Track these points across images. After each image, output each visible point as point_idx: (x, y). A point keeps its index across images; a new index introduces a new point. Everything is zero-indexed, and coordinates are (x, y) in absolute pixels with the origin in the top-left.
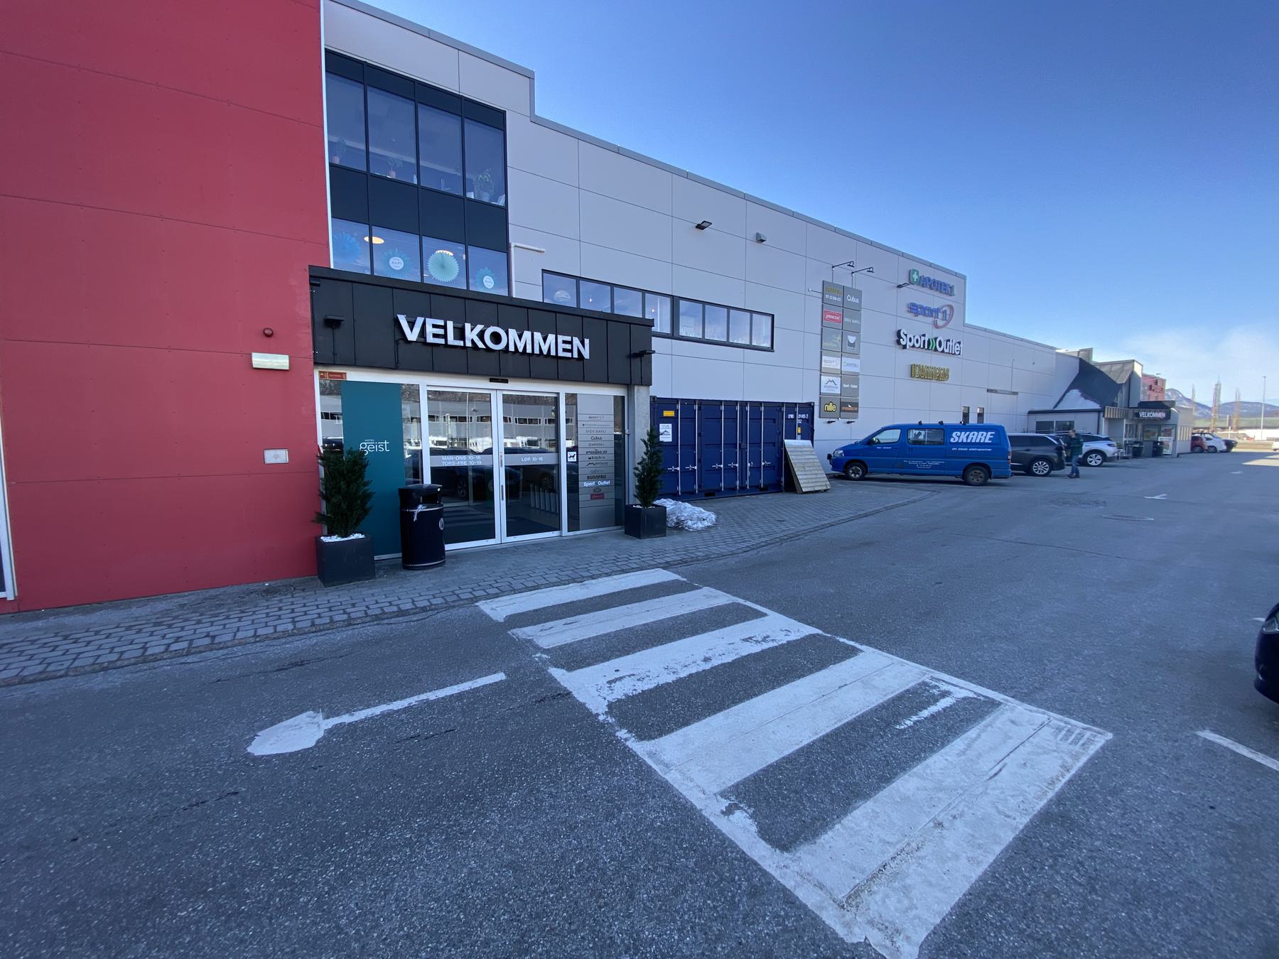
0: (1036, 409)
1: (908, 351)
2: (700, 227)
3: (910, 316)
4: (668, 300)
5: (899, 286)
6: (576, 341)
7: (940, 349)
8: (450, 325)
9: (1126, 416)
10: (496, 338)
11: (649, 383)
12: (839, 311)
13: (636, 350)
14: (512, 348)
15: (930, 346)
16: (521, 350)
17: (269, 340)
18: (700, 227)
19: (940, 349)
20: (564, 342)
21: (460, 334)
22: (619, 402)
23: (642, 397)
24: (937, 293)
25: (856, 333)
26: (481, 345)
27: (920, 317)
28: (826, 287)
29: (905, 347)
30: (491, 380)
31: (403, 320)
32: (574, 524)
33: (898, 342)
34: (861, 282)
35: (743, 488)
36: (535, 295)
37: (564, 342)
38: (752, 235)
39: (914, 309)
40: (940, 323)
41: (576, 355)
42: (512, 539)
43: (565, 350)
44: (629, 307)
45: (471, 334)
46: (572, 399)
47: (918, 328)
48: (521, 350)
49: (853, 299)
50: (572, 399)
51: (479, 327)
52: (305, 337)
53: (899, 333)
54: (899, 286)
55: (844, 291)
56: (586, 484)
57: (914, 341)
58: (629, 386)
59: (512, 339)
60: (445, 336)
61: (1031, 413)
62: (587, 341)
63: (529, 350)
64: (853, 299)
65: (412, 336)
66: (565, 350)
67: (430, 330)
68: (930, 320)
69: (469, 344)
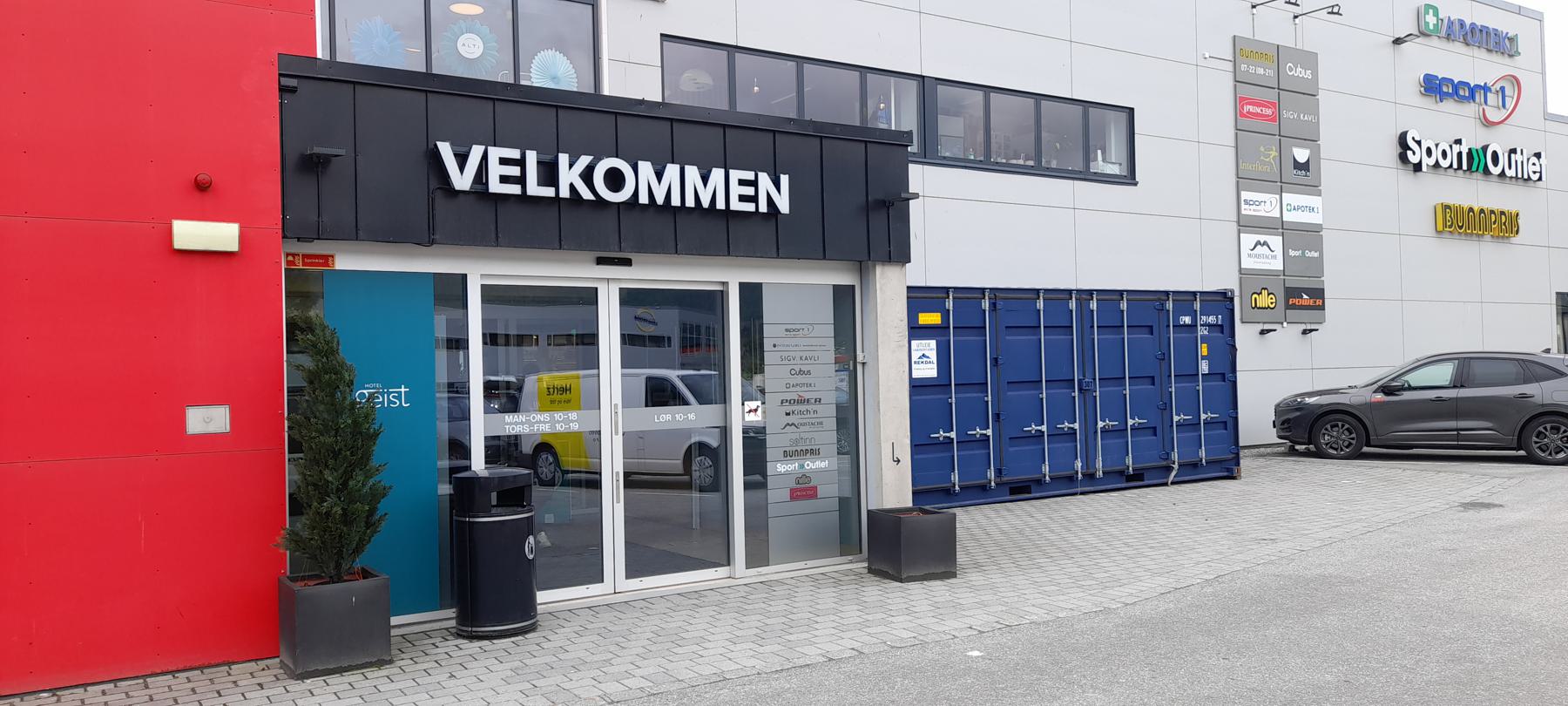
1: (1426, 176)
3: (1428, 102)
5: (1398, 41)
7: (1496, 171)
8: (532, 158)
10: (615, 179)
11: (899, 254)
14: (644, 199)
15: (1475, 163)
17: (203, 198)
19: (1496, 171)
21: (549, 174)
22: (843, 298)
23: (888, 290)
24: (1483, 54)
25: (1311, 140)
26: (586, 194)
27: (1449, 106)
29: (1418, 167)
30: (600, 261)
31: (445, 150)
32: (757, 557)
33: (1403, 158)
39: (1433, 87)
40: (1494, 115)
41: (763, 208)
42: (636, 583)
45: (569, 176)
46: (752, 295)
49: (1299, 72)
50: (752, 295)
51: (584, 161)
52: (268, 188)
54: (1398, 41)
56: (782, 468)
57: (1437, 154)
59: (646, 181)
60: (521, 180)
62: (784, 179)
63: (676, 201)
64: (1299, 72)
65: (462, 181)
67: (495, 170)
68: (1471, 109)
69: (565, 193)
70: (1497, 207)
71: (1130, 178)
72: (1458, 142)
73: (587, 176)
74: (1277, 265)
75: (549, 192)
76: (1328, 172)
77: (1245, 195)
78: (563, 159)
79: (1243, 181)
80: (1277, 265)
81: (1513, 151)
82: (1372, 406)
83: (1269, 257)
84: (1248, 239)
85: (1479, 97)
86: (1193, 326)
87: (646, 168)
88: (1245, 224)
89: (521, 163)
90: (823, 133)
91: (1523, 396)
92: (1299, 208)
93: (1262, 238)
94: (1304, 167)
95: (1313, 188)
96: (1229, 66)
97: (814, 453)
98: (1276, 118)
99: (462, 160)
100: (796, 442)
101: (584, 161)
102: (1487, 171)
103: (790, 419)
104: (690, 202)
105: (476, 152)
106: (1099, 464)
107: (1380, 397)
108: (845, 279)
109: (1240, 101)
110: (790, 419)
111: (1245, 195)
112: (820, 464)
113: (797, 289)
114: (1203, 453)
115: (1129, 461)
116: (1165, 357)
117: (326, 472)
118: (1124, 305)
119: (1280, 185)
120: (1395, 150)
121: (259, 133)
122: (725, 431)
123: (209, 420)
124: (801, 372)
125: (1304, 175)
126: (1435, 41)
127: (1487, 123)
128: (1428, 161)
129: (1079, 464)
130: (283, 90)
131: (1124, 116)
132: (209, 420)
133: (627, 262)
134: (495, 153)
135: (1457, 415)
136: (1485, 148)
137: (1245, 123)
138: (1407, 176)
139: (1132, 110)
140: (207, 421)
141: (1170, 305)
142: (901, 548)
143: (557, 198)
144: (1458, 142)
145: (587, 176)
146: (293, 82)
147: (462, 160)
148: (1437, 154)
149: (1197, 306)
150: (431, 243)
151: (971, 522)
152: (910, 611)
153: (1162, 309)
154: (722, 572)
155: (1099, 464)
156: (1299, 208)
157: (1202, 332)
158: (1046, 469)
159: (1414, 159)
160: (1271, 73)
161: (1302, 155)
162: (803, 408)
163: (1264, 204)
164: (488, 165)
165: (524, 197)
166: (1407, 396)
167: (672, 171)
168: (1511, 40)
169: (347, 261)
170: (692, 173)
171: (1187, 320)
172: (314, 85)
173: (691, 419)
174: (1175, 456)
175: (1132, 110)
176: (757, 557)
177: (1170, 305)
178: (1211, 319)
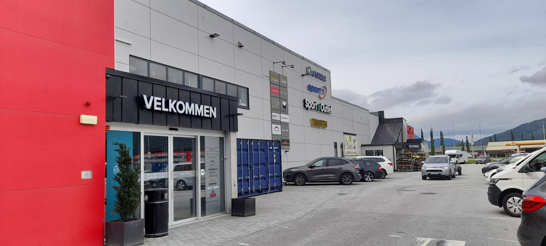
0: (364, 143)
1: (309, 111)
2: (241, 46)
3: (307, 91)
4: (196, 77)
5: (303, 75)
6: (211, 108)
7: (322, 110)
8: (164, 100)
9: (404, 148)
10: (181, 107)
11: (235, 130)
12: (278, 87)
13: (231, 113)
14: (187, 113)
15: (318, 108)
16: (190, 113)
17: (88, 107)
18: (212, 36)
19: (322, 110)
20: (158, 101)
21: (167, 106)
22: (221, 139)
23: (233, 138)
24: (319, 80)
25: (286, 100)
26: (175, 111)
27: (313, 93)
28: (272, 74)
29: (307, 109)
30: (171, 129)
31: (145, 97)
32: (204, 213)
33: (304, 106)
34: (287, 72)
35: (252, 192)
36: (126, 69)
37: (158, 101)
38: (236, 43)
39: (311, 88)
40: (322, 96)
41: (211, 116)
42: (176, 222)
43: (158, 106)
44: (232, 92)
45: (171, 106)
46: (202, 138)
47: (312, 98)
48: (190, 113)
49: (283, 82)
50: (202, 138)
51: (175, 101)
52: (103, 106)
53: (304, 100)
54: (303, 75)
55: (279, 76)
56: (209, 188)
57: (311, 105)
58: (226, 133)
59: (189, 108)
60: (161, 106)
61: (362, 146)
62: (215, 108)
63: (193, 114)
64: (283, 82)
65: (149, 106)
66: (158, 106)
67: (156, 103)
68: (317, 94)
69: (170, 111)
70: (323, 120)
71: (248, 108)
72: (315, 102)
73: (175, 106)
74: (280, 133)
75: (167, 110)
76: (290, 108)
77: (273, 114)
78: (170, 101)
79: (273, 110)
80: (280, 133)
81: (325, 106)
82: (307, 171)
83: (278, 131)
84: (274, 126)
85: (319, 91)
86: (273, 149)
87: (187, 104)
88: (273, 122)
89: (161, 101)
90: (221, 97)
91: (341, 168)
92: (284, 118)
93: (277, 126)
94: (285, 107)
95: (286, 113)
96: (269, 78)
97: (215, 184)
98: (279, 93)
99: (148, 100)
100: (212, 181)
101: (175, 101)
102: (321, 111)
103: (211, 174)
104: (196, 114)
105: (152, 98)
106: (254, 188)
107: (309, 169)
108: (221, 136)
109: (271, 88)
110: (211, 174)
111: (273, 114)
112: (217, 187)
113: (212, 137)
114: (242, 190)
115: (260, 187)
116: (267, 158)
117: (130, 189)
118: (259, 144)
119: (280, 112)
120: (303, 104)
121: (100, 90)
122: (195, 178)
123: (86, 175)
124: (213, 161)
125: (284, 109)
126: (310, 76)
127: (320, 98)
128: (310, 107)
129: (250, 188)
130: (107, 78)
131: (246, 90)
132: (86, 175)
133: (177, 130)
134: (156, 98)
135: (327, 173)
136: (320, 104)
137: (273, 94)
138: (305, 111)
139: (248, 89)
140: (86, 175)
141: (268, 144)
142: (241, 208)
143: (169, 112)
144: (315, 102)
145: (175, 106)
146: (110, 76)
147: (148, 100)
148: (311, 105)
149: (273, 144)
150: (138, 123)
151: (259, 200)
152: (245, 225)
153: (266, 145)
154: (195, 218)
155: (254, 188)
156: (284, 118)
157: (274, 151)
158: (260, 187)
159: (307, 106)
160: (278, 81)
161: (284, 104)
162: (213, 171)
163: (277, 117)
164: (153, 102)
165: (161, 112)
166: (315, 168)
167: (193, 105)
168: (325, 77)
169: (112, 128)
170: (197, 105)
171: (271, 148)
172: (114, 77)
173: (188, 174)
174: (269, 185)
175: (248, 89)
176: (204, 213)
177: (268, 144)
178: (276, 148)
